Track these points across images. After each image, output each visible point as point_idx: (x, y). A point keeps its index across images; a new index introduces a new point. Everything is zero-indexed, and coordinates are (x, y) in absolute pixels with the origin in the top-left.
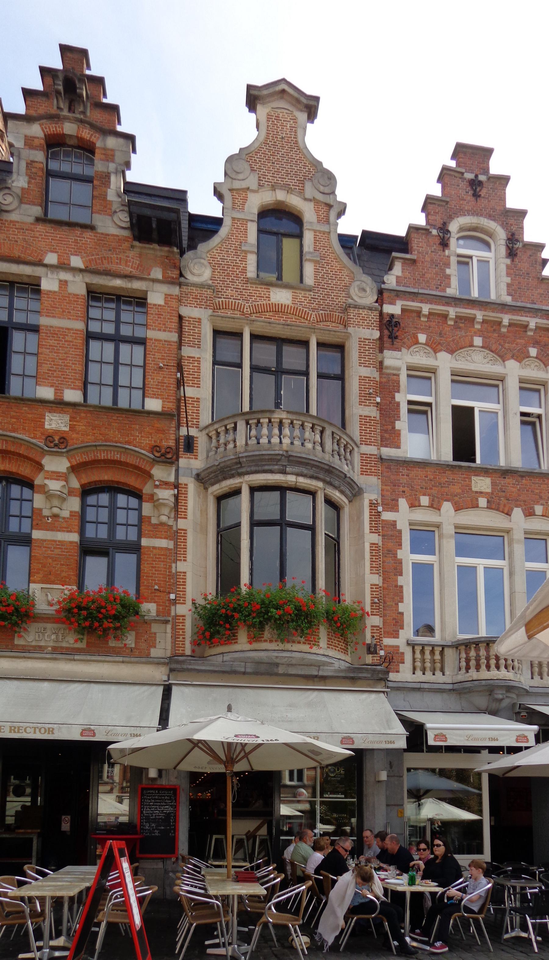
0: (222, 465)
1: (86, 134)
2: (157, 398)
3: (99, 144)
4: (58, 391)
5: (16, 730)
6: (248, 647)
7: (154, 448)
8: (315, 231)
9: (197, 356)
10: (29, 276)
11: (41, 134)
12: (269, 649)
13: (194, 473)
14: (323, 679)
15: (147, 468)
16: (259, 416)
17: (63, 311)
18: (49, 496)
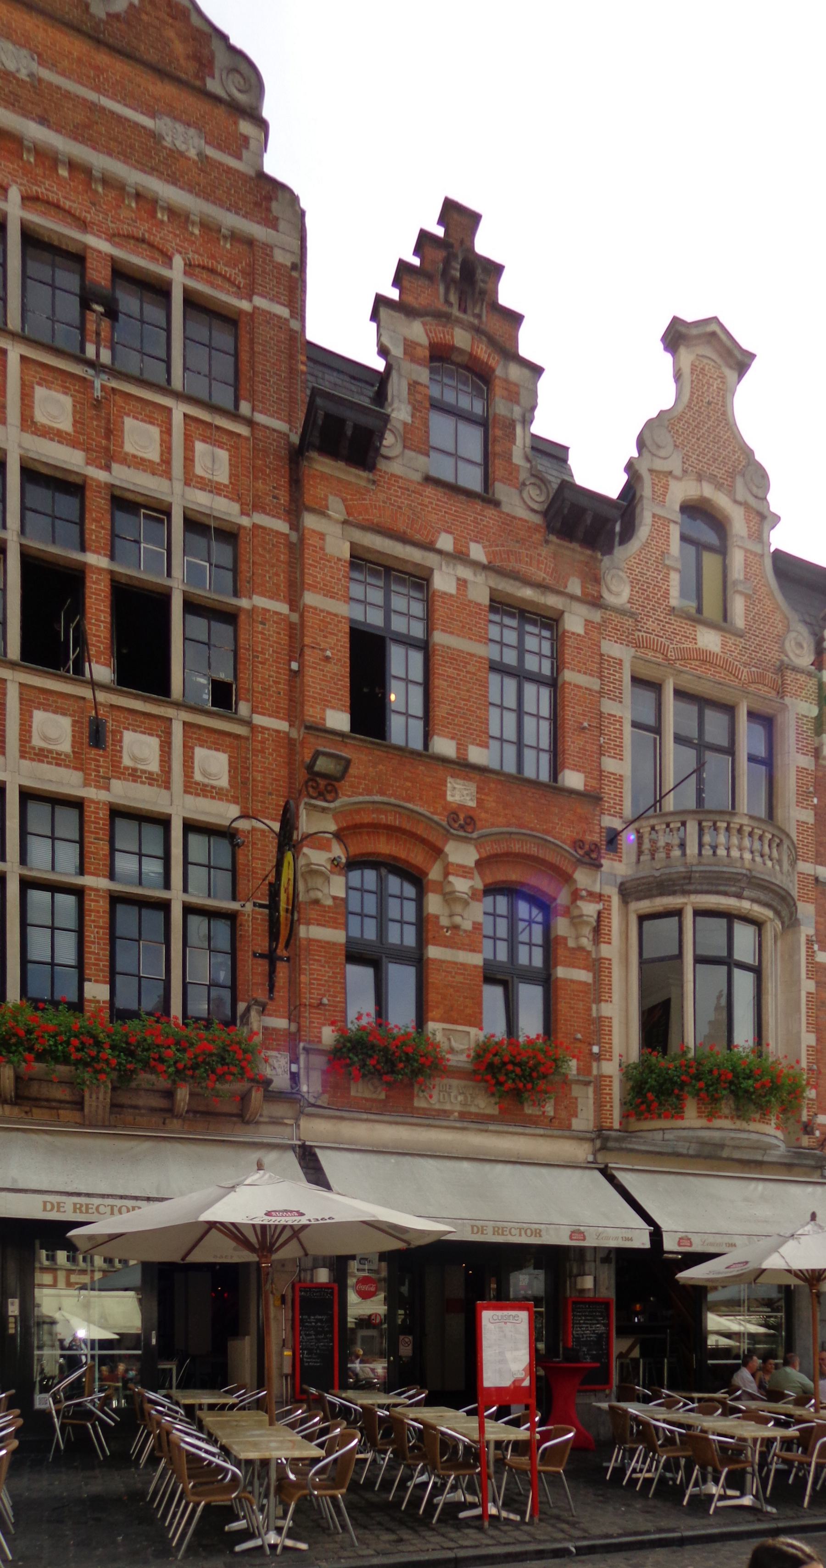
0: (664, 877)
1: (483, 351)
2: (578, 771)
3: (499, 372)
4: (461, 748)
5: (84, 1209)
6: (703, 1122)
7: (578, 844)
8: (746, 551)
9: (619, 714)
10: (416, 565)
11: (425, 341)
12: (725, 1128)
13: (619, 881)
14: (758, 1165)
15: (570, 871)
16: (717, 818)
17: (463, 627)
18: (450, 897)
